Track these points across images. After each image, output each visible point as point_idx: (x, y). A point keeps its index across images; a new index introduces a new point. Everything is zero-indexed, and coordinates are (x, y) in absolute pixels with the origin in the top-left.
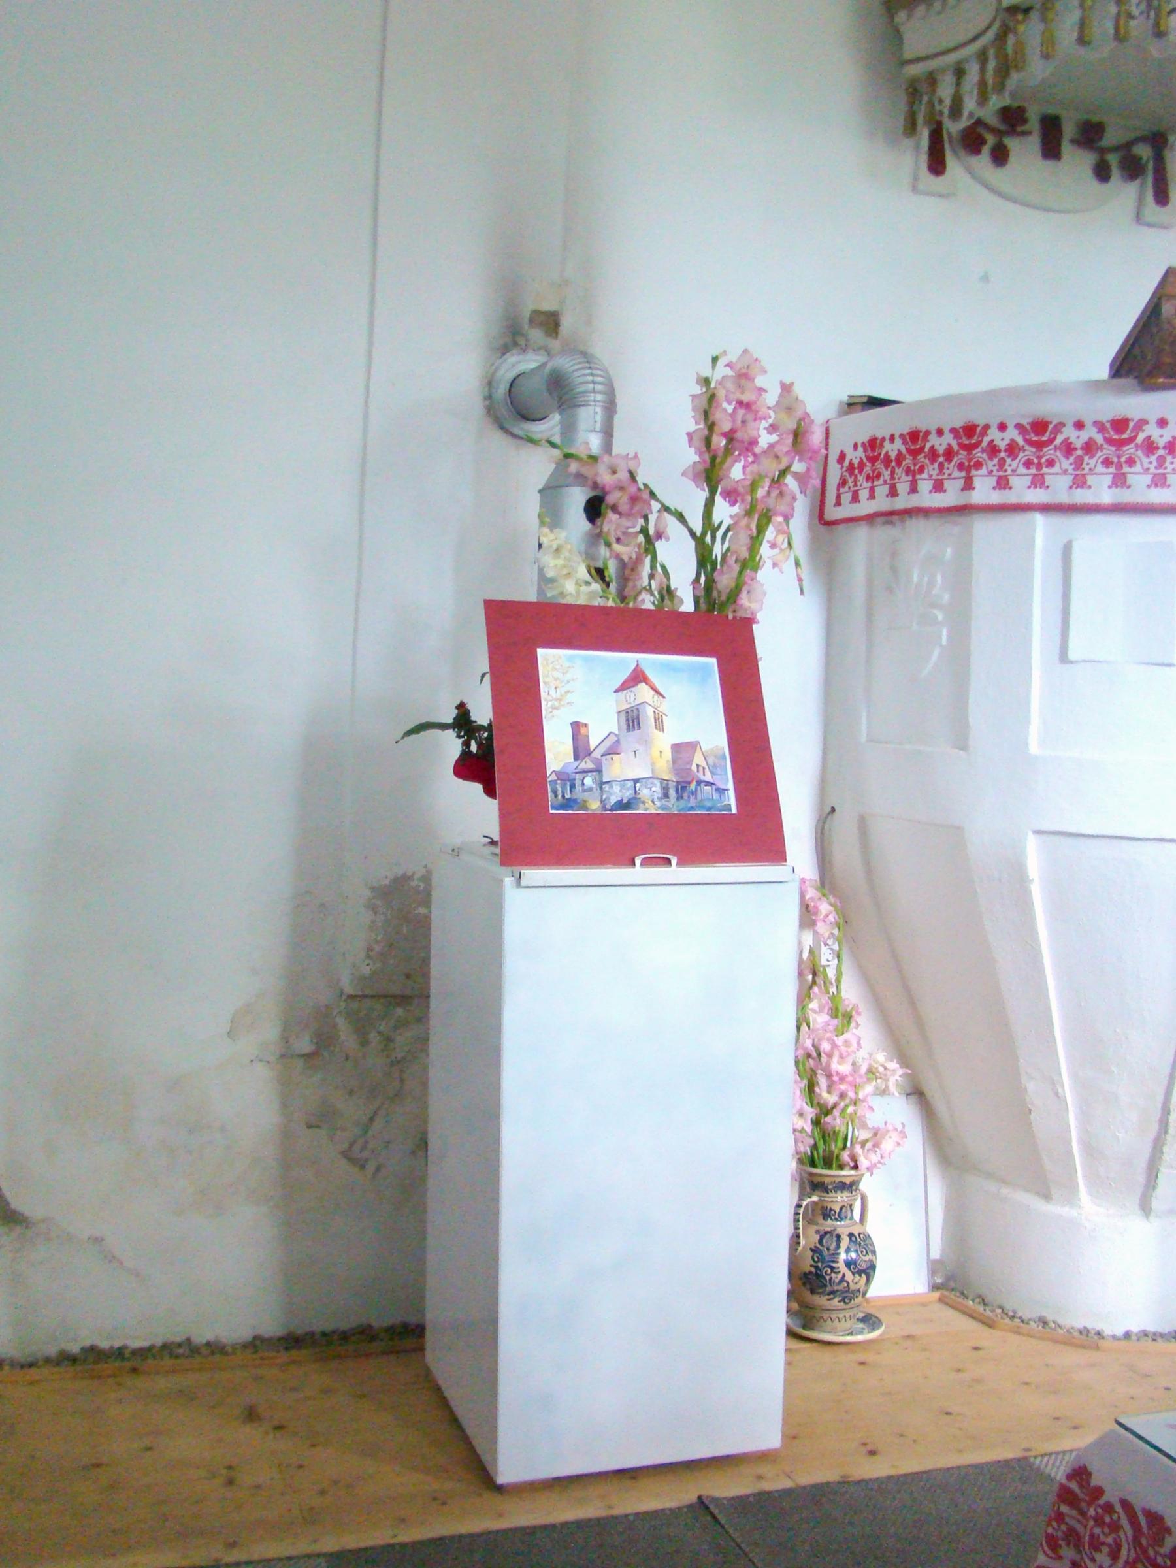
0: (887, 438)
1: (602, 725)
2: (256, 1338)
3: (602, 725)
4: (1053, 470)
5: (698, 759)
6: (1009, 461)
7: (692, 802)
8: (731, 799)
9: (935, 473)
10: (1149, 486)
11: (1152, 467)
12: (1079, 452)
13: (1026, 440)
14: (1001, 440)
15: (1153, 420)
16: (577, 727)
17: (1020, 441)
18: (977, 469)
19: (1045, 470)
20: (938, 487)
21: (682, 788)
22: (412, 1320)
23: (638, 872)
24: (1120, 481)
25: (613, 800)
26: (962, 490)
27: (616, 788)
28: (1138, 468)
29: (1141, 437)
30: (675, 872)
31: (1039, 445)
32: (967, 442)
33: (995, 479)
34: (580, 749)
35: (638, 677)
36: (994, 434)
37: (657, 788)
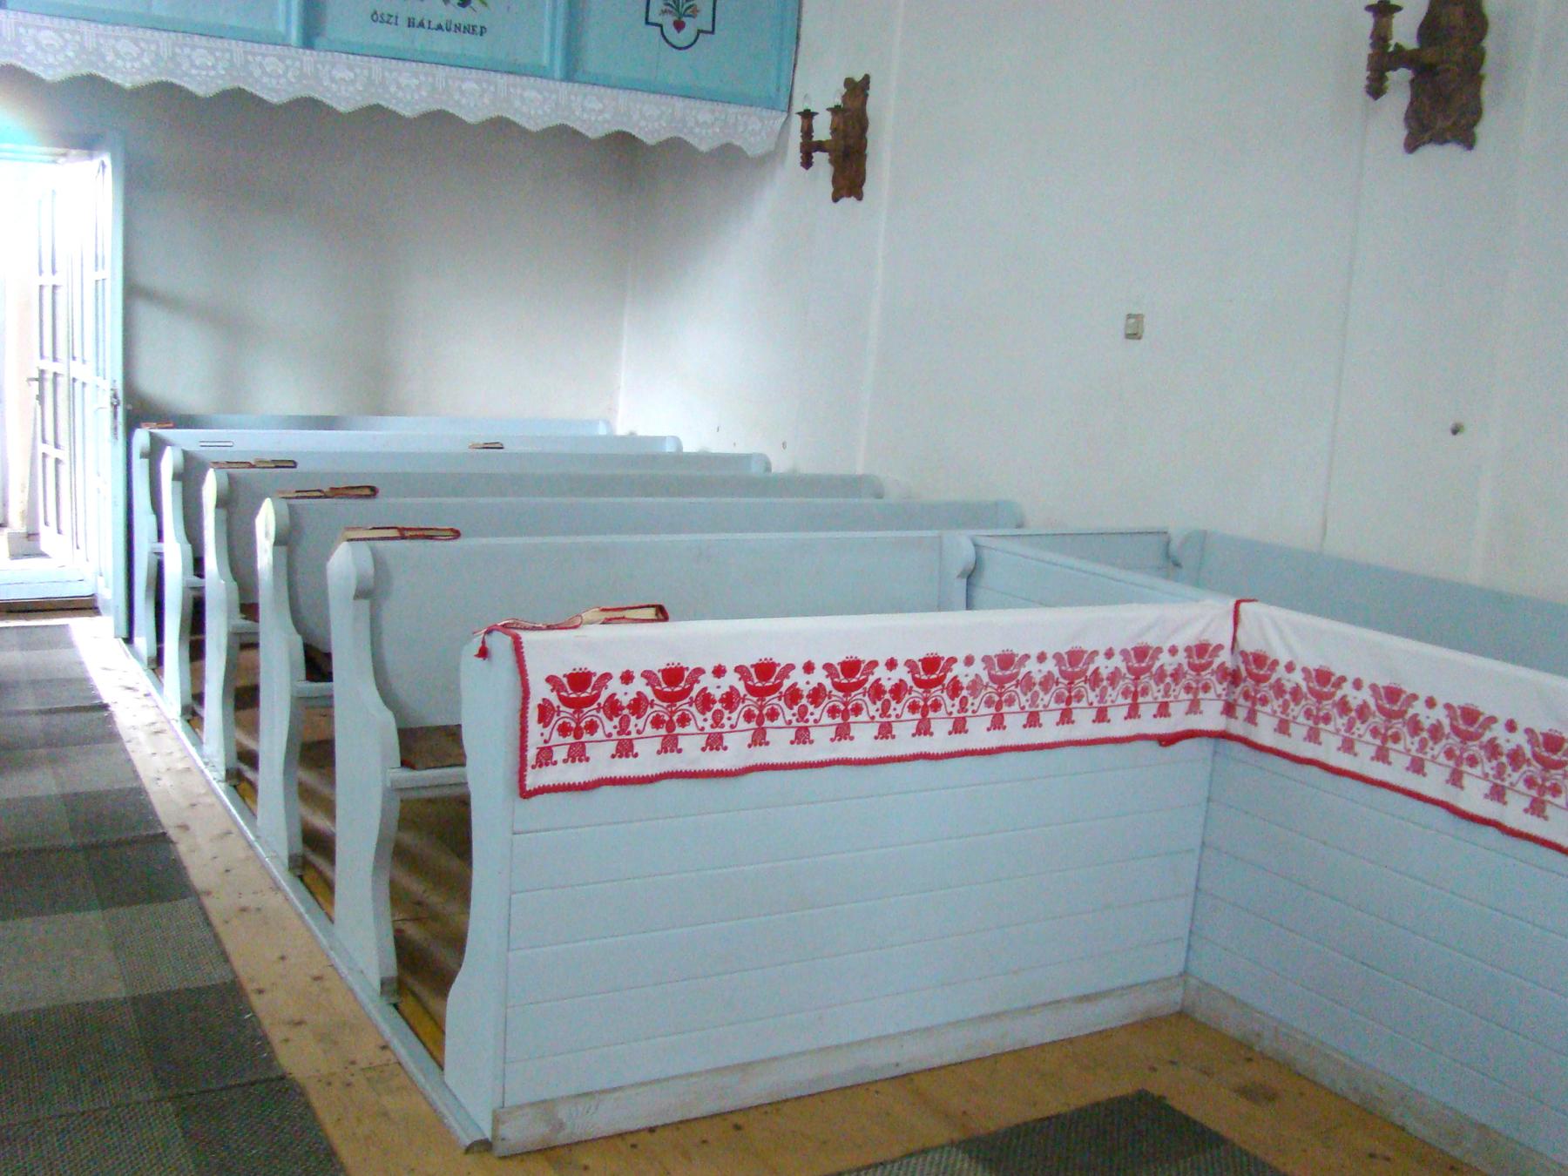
0: (1350, 680)
4: (1208, 696)
6: (893, 703)
9: (1414, 748)
10: (703, 749)
11: (707, 726)
12: (718, 706)
13: (747, 687)
14: (1428, 717)
15: (617, 674)
17: (648, 692)
18: (772, 720)
19: (586, 737)
24: (670, 745)
26: (659, 752)
28: (691, 728)
29: (787, 683)
31: (1466, 737)
32: (925, 677)
33: (793, 731)
36: (707, 681)
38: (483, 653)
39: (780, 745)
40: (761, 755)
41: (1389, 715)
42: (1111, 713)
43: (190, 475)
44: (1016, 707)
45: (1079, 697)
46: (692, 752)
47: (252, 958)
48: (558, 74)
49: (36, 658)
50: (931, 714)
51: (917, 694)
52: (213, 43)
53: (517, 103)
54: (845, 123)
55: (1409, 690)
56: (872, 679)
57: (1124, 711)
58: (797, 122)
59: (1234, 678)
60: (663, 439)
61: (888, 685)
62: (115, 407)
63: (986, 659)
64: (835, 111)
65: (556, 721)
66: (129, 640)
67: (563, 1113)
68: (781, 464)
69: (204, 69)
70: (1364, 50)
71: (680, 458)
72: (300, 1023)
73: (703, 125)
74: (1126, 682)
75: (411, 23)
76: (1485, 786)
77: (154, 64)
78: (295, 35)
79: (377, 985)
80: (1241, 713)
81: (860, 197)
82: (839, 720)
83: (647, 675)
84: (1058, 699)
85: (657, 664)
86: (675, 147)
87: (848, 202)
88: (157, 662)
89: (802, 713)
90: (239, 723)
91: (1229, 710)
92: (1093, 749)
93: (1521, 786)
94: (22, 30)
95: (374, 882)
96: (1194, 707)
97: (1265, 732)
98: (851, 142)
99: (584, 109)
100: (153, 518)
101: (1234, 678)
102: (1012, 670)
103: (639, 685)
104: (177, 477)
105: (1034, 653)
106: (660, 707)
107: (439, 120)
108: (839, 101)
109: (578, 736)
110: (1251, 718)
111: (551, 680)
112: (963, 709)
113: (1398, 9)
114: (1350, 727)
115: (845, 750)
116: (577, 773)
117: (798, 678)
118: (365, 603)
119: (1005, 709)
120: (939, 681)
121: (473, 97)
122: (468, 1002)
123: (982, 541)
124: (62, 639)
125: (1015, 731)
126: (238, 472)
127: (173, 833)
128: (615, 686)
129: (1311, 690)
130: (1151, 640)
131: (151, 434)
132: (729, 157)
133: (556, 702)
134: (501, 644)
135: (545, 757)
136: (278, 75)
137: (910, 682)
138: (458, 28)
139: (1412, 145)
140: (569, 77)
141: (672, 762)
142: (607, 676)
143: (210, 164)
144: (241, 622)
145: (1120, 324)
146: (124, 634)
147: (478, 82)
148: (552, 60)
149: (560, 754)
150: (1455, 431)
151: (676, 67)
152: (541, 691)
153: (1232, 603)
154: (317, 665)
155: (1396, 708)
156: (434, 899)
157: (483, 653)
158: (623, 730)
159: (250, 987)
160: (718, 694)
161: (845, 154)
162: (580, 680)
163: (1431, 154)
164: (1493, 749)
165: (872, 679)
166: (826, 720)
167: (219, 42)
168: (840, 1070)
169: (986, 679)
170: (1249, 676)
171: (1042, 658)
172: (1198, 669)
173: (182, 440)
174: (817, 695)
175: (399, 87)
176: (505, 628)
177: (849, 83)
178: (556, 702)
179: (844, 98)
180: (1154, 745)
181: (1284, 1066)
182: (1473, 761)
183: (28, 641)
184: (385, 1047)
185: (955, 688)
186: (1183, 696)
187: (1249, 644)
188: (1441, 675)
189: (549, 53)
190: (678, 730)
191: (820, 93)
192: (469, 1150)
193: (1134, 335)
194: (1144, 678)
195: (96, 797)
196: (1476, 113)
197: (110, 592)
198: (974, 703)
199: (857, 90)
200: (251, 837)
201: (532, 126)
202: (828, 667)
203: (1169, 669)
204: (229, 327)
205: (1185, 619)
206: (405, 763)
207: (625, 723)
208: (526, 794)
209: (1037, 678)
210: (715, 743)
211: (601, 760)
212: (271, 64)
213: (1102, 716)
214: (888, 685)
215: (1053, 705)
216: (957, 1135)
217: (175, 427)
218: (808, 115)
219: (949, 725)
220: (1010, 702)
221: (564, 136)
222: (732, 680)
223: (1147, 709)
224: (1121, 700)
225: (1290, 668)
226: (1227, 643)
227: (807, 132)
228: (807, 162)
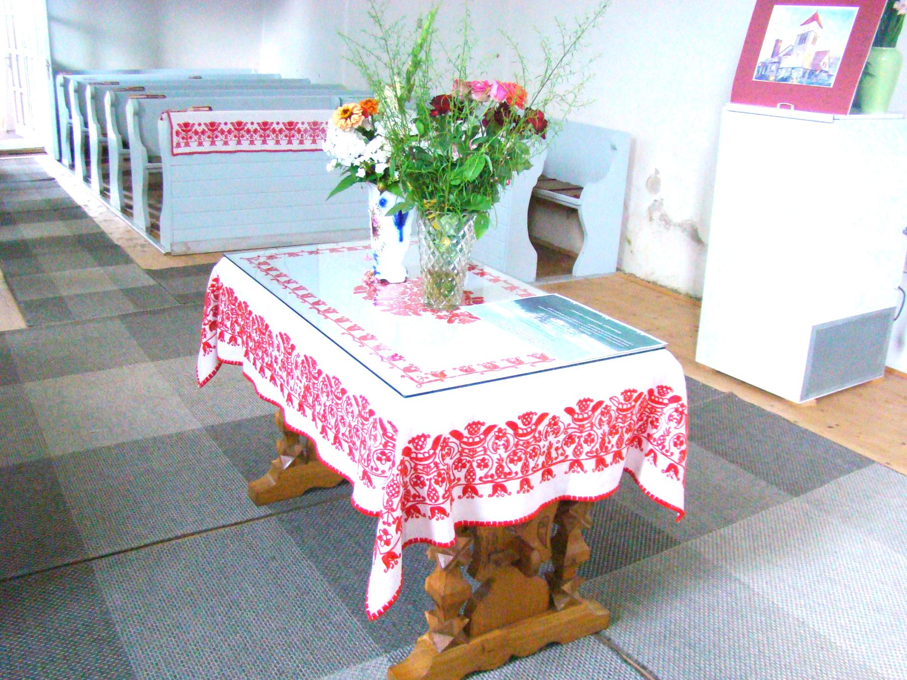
1: (789, 40)
3: (789, 40)
5: (826, 60)
7: (814, 81)
8: (832, 81)
16: (778, 41)
21: (812, 73)
22: (699, 296)
23: (777, 110)
25: (780, 77)
27: (784, 71)
30: (792, 112)
31: (213, 131)
34: (775, 53)
35: (815, 18)
37: (801, 73)
39: (245, 145)
40: (239, 148)
43: (80, 90)
49: (25, 167)
63: (309, 123)
66: (60, 161)
67: (190, 245)
68: (314, 81)
83: (205, 124)
88: (72, 166)
89: (251, 137)
90: (104, 182)
100: (67, 110)
103: (203, 127)
104: (76, 91)
106: (209, 133)
111: (179, 125)
115: (265, 147)
116: (187, 150)
117: (249, 126)
120: (293, 129)
126: (97, 86)
134: (165, 116)
135: (178, 145)
141: (213, 148)
144: (102, 138)
149: (183, 144)
152: (176, 128)
154: (125, 145)
162: (186, 125)
173: (74, 80)
174: (256, 131)
185: (299, 131)
197: (51, 145)
198: (306, 136)
207: (200, 137)
210: (226, 143)
211: (194, 147)
219: (298, 142)
222: (230, 126)
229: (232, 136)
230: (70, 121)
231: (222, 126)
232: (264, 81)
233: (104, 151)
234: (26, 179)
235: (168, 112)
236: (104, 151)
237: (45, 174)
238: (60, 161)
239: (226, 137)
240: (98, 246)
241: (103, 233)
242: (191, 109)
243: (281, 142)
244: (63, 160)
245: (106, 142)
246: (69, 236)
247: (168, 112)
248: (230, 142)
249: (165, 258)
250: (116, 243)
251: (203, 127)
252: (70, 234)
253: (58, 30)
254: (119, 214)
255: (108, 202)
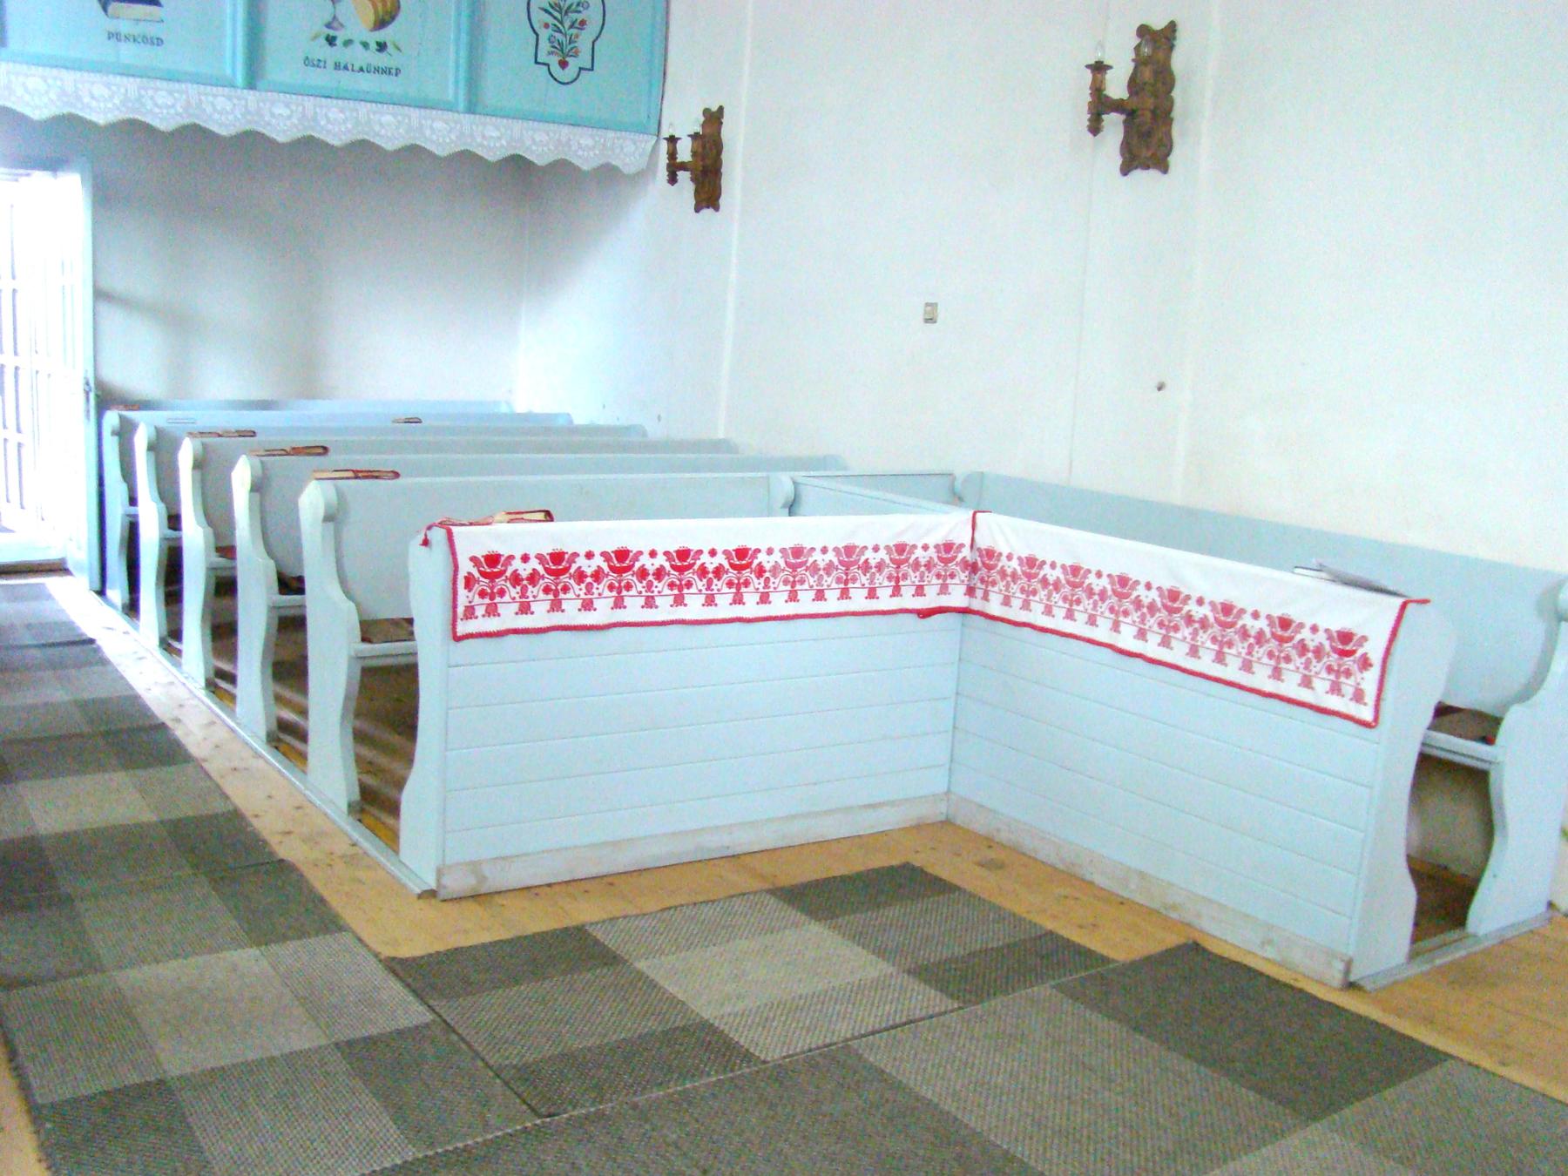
0: (1143, 583)
2: (947, 823)
9: (1244, 652)
15: (518, 556)
19: (498, 599)
20: (588, 606)
28: (570, 595)
29: (638, 565)
36: (581, 562)
38: (426, 543)
41: (1074, 585)
42: (879, 592)
43: (163, 448)
44: (806, 586)
45: (854, 580)
46: (572, 613)
47: (245, 796)
48: (462, 106)
49: (22, 607)
50: (743, 589)
51: (732, 574)
52: (171, 85)
53: (428, 133)
54: (704, 147)
55: (1085, 567)
56: (699, 563)
57: (890, 591)
58: (664, 146)
59: (973, 568)
60: (557, 415)
61: (711, 568)
62: (87, 393)
63: (783, 551)
64: (695, 137)
65: (477, 588)
66: (101, 592)
67: (487, 870)
68: (655, 431)
69: (166, 108)
70: (1086, 97)
71: (574, 430)
72: (289, 833)
73: (585, 149)
74: (890, 569)
75: (337, 66)
76: (1134, 630)
77: (123, 103)
78: (240, 79)
79: (345, 807)
80: (979, 593)
81: (717, 208)
82: (676, 592)
83: (540, 557)
84: (839, 580)
85: (546, 550)
86: (562, 168)
87: (707, 213)
88: (132, 608)
89: (649, 586)
91: (971, 591)
92: (867, 618)
93: (1156, 628)
94: (13, 78)
95: (342, 723)
96: (944, 589)
97: (994, 607)
98: (708, 162)
99: (484, 137)
100: (124, 487)
101: (973, 568)
102: (803, 559)
104: (151, 448)
105: (819, 547)
107: (363, 148)
108: (699, 129)
109: (492, 598)
110: (986, 597)
111: (474, 559)
112: (766, 586)
113: (1109, 67)
114: (1049, 596)
116: (492, 624)
117: (645, 561)
118: (331, 525)
119: (798, 587)
120: (748, 566)
121: (390, 128)
122: (419, 794)
123: (800, 480)
124: (41, 594)
125: (807, 603)
127: (170, 724)
128: (516, 564)
129: (1024, 573)
130: (908, 539)
131: (121, 417)
132: (608, 175)
133: (477, 575)
134: (438, 535)
135: (470, 613)
136: (225, 112)
137: (727, 566)
138: (377, 70)
139: (1126, 170)
140: (471, 109)
141: (558, 619)
142: (511, 557)
143: (160, 180)
145: (920, 311)
146: (97, 586)
147: (395, 115)
148: (456, 94)
149: (480, 611)
150: (1160, 389)
151: (563, 100)
152: (466, 567)
153: (971, 513)
154: (291, 584)
155: (1348, 648)
156: (383, 760)
157: (426, 543)
158: (523, 595)
159: (248, 814)
160: (589, 571)
161: (704, 171)
162: (493, 559)
163: (1138, 175)
164: (1138, 604)
165: (699, 563)
166: (667, 591)
167: (177, 86)
168: (684, 849)
169: (783, 565)
170: (982, 566)
171: (824, 550)
172: (946, 561)
175: (328, 121)
176: (441, 525)
177: (706, 112)
178: (477, 575)
179: (703, 126)
180: (913, 618)
181: (1016, 851)
182: (1126, 613)
183: (14, 595)
184: (354, 845)
185: (760, 571)
186: (935, 581)
187: (983, 542)
188: (1108, 555)
189: (453, 90)
190: (562, 596)
191: (684, 122)
192: (420, 896)
193: (930, 320)
194: (904, 568)
195: (102, 702)
196: (1169, 148)
197: (81, 553)
198: (776, 582)
199: (714, 119)
200: (232, 724)
201: (441, 152)
202: (666, 553)
203: (923, 561)
204: (177, 322)
205: (939, 525)
206: (364, 640)
207: (524, 589)
208: (457, 639)
209: (822, 565)
211: (508, 616)
212: (221, 102)
213: (872, 594)
214: (711, 568)
215: (834, 585)
216: (767, 886)
217: (139, 409)
218: (672, 140)
219: (757, 597)
220: (802, 582)
221: (466, 158)
222: (599, 561)
223: (908, 591)
224: (886, 583)
225: (1009, 557)
226: (967, 542)
227: (672, 155)
228: (673, 179)
229: (602, 587)
230: (132, 510)
231: (581, 562)
232: (548, 430)
233: (224, 588)
234: (28, 640)
235: (446, 526)
236: (224, 588)
237: (70, 625)
238: (101, 592)
239: (589, 588)
240: (227, 862)
241: (236, 816)
242: (500, 516)
243: (718, 599)
244: (109, 592)
245: (180, 539)
246: (149, 825)
247: (446, 526)
248: (597, 603)
249: (430, 911)
250: (283, 852)
251: (534, 564)
252: (148, 817)
253: (114, 318)
254: (202, 693)
255: (178, 665)
